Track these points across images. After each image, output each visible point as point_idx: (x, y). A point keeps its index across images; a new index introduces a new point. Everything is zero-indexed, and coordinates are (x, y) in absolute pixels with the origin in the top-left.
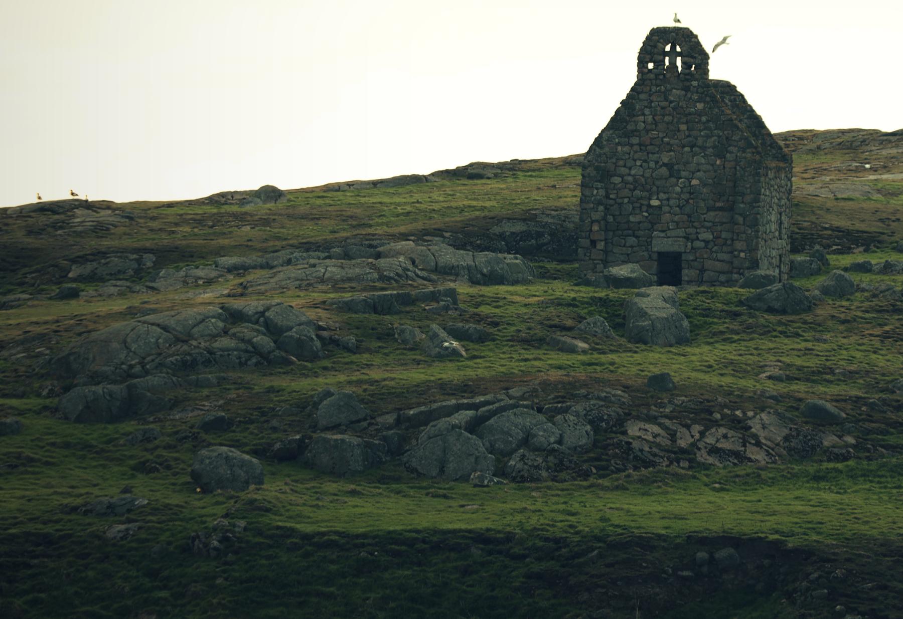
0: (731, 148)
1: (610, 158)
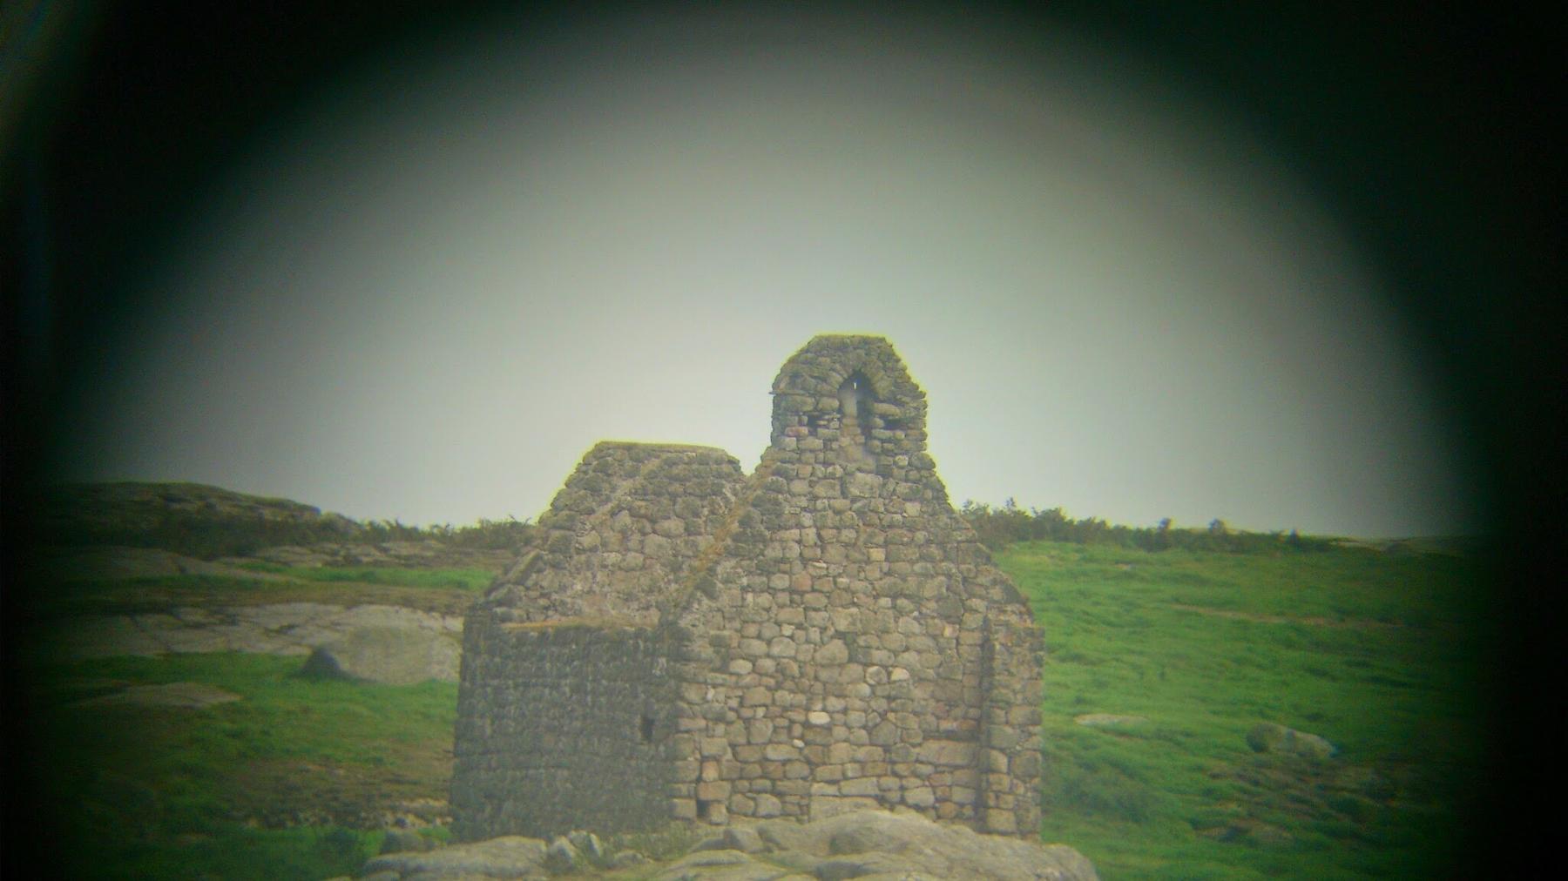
0: (976, 603)
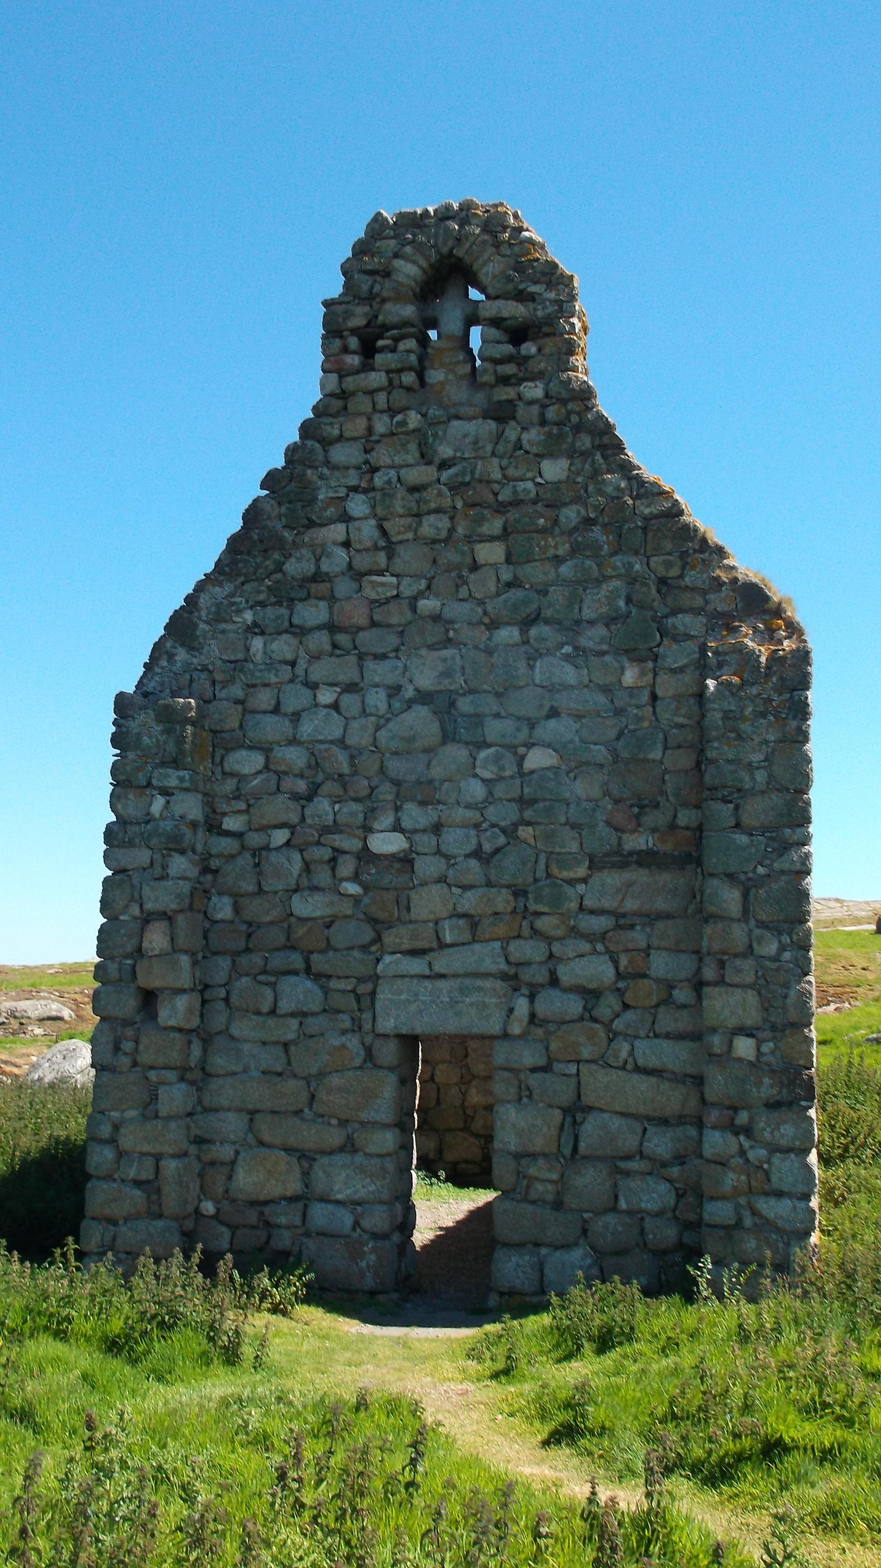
0: (683, 622)
1: (225, 684)
